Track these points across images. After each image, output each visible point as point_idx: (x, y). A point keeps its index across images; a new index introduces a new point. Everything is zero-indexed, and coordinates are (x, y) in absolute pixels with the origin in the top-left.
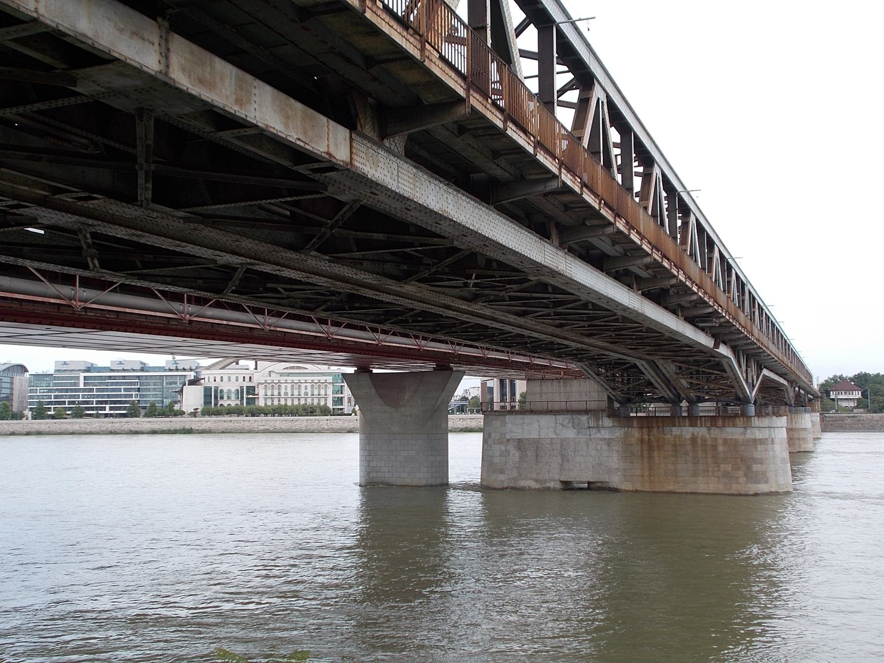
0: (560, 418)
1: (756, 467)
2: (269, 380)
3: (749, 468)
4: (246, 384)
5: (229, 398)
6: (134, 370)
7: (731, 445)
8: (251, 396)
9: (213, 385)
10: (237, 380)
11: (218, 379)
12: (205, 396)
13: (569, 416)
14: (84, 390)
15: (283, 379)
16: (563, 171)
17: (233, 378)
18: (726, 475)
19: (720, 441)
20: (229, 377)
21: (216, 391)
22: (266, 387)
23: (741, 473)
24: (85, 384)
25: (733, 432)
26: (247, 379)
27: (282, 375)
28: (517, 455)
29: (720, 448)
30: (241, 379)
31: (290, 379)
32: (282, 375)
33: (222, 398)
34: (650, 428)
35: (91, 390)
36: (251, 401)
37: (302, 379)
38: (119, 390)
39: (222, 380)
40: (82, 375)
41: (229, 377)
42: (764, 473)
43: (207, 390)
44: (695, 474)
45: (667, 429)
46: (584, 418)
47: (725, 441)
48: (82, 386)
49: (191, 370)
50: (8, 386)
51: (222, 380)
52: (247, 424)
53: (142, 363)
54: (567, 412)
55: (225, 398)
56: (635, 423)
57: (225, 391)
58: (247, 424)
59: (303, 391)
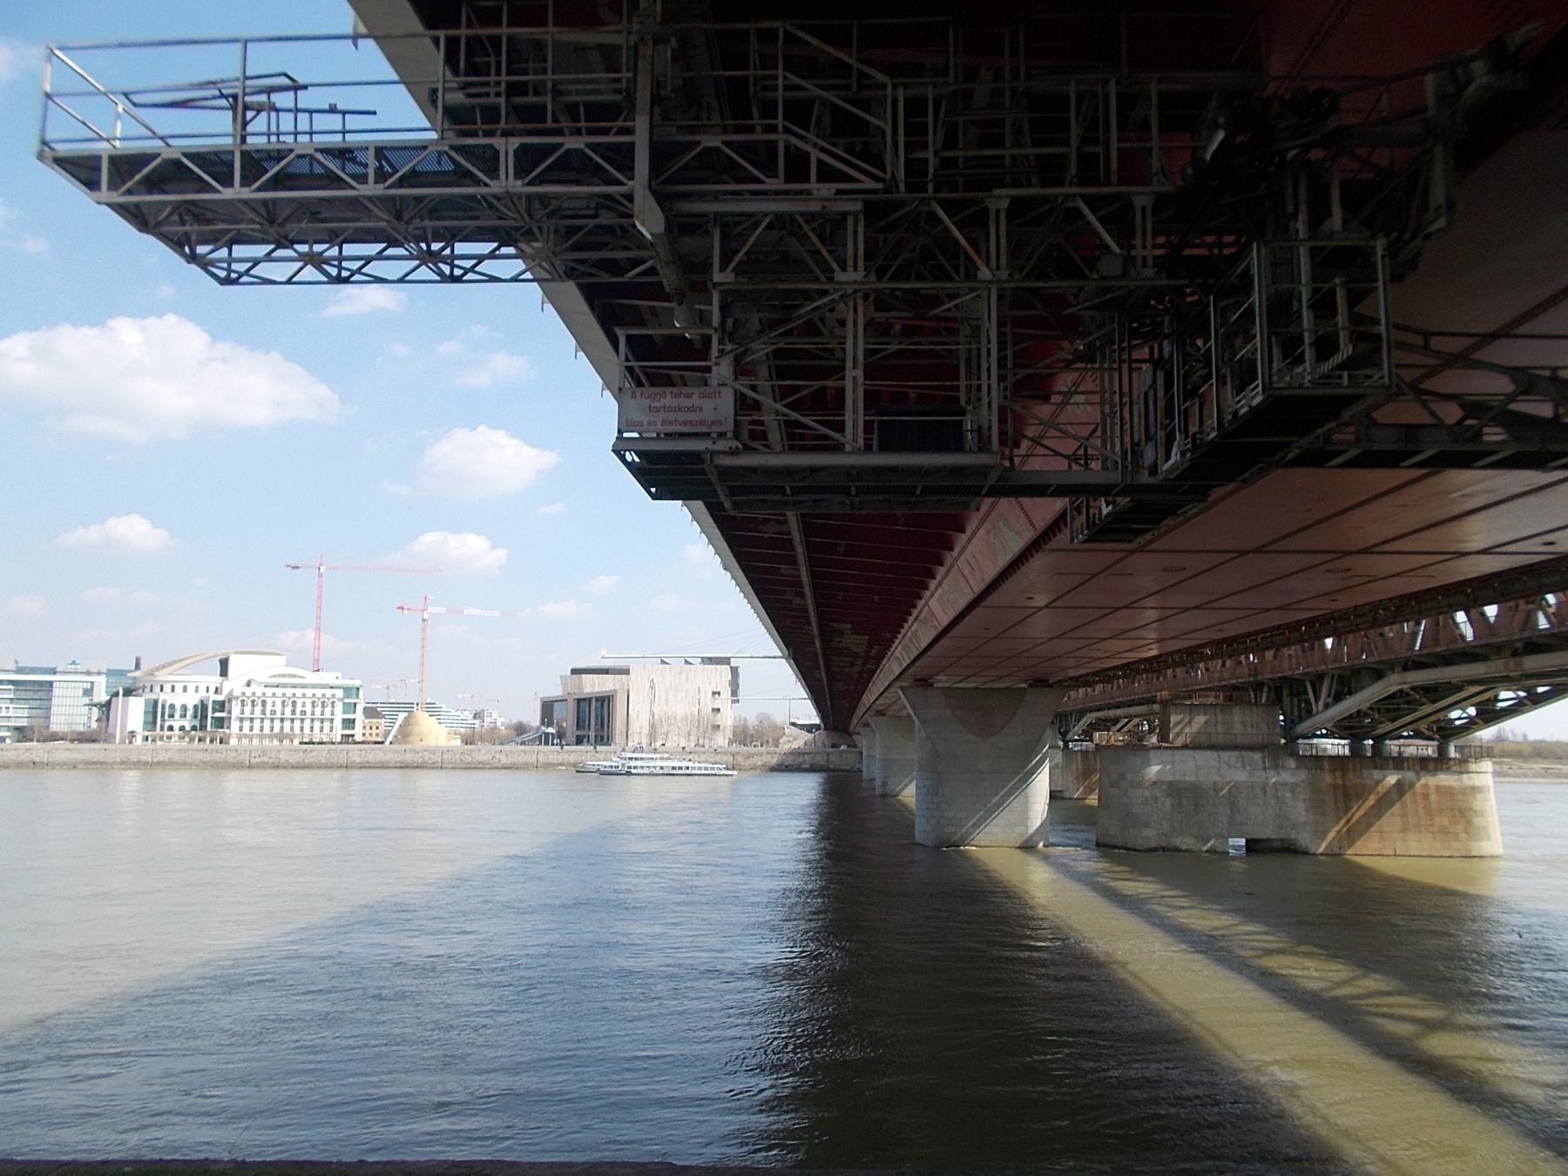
0: (1225, 755)
1: (1477, 821)
3: (1469, 822)
13: (1237, 753)
15: (269, 691)
16: (1434, 406)
17: (191, 688)
18: (1444, 831)
19: (1432, 791)
23: (1460, 828)
25: (1444, 779)
26: (212, 690)
28: (1168, 801)
29: (1433, 797)
31: (279, 691)
33: (171, 716)
34: (1344, 770)
37: (299, 692)
44: (1404, 830)
46: (1257, 756)
47: (1438, 788)
49: (99, 673)
54: (1236, 748)
55: (177, 716)
56: (1326, 766)
57: (178, 707)
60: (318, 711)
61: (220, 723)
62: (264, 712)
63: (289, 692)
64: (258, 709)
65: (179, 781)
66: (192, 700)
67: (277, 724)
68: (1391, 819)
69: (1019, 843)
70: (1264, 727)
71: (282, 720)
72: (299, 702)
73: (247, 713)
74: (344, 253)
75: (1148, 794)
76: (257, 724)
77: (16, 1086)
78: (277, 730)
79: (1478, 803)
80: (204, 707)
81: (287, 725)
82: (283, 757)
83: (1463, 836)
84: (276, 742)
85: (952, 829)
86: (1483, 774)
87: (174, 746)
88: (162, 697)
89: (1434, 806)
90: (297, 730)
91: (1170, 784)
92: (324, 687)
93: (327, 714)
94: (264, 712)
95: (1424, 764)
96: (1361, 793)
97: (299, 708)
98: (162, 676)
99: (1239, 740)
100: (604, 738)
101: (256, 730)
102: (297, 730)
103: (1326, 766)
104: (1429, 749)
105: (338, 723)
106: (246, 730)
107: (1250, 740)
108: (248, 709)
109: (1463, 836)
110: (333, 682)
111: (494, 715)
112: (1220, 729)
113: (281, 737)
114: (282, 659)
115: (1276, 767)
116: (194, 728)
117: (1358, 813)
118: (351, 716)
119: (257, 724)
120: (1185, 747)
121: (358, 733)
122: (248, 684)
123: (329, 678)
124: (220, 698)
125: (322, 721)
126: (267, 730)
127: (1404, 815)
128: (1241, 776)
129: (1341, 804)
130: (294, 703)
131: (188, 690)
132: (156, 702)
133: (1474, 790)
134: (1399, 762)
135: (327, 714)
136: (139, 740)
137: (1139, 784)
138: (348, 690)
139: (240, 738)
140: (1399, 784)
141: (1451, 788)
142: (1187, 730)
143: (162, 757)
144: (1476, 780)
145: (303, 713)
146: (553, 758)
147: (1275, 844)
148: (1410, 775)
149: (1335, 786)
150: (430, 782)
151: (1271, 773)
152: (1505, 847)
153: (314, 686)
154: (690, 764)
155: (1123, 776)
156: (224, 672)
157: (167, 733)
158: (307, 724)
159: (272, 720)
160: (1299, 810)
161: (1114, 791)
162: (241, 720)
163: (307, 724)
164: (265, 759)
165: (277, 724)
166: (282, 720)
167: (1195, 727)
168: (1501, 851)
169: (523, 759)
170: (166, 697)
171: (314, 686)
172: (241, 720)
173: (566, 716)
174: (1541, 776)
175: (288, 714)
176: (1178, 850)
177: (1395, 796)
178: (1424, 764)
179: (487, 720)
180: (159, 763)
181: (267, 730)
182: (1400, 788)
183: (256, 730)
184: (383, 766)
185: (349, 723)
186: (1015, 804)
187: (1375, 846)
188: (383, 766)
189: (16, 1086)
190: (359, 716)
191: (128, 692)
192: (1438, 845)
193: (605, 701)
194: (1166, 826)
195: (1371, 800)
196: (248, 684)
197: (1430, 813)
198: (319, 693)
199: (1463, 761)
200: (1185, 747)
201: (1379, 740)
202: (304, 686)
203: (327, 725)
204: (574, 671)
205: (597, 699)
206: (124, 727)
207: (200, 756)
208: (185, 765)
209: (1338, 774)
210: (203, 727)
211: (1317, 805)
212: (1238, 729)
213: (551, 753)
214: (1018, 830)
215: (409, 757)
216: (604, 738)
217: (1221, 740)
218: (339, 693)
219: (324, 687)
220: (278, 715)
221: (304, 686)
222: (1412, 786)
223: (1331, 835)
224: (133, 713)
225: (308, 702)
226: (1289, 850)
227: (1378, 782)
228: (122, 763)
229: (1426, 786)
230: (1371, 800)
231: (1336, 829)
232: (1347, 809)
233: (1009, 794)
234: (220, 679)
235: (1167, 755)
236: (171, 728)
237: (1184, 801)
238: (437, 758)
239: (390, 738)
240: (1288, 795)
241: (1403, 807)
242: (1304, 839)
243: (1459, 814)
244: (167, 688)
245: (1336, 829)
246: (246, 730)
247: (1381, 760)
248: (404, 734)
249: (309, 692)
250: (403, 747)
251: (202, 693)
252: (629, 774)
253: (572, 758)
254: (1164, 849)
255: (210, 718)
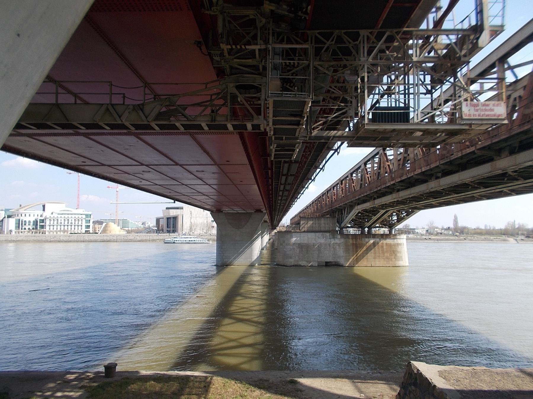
0: (317, 234)
1: (398, 255)
3: (396, 255)
4: (40, 218)
5: (29, 225)
7: (390, 246)
13: (321, 233)
15: (59, 216)
17: (32, 215)
18: (387, 258)
19: (385, 245)
21: (22, 221)
23: (393, 257)
25: (389, 241)
26: (39, 216)
28: (298, 250)
29: (385, 247)
31: (63, 216)
33: (25, 224)
34: (356, 239)
37: (70, 216)
42: (401, 257)
44: (375, 258)
45: (363, 239)
46: (328, 234)
47: (386, 244)
49: (2, 210)
50: (311, 207)
55: (27, 224)
56: (350, 237)
57: (27, 222)
60: (77, 222)
61: (42, 227)
62: (57, 223)
64: (55, 222)
65: (28, 248)
66: (32, 219)
67: (62, 227)
68: (371, 255)
69: (249, 264)
70: (331, 225)
71: (64, 226)
72: (59, 219)
73: (52, 223)
74: (426, 76)
75: (291, 247)
76: (55, 227)
78: (62, 229)
79: (399, 249)
80: (37, 221)
81: (66, 227)
82: (62, 238)
83: (394, 260)
84: (62, 233)
85: (227, 260)
86: (403, 239)
87: (25, 235)
88: (21, 218)
89: (385, 250)
90: (69, 229)
91: (299, 244)
92: (78, 214)
93: (80, 223)
94: (57, 223)
95: (383, 236)
96: (362, 246)
97: (70, 222)
98: (21, 211)
99: (323, 229)
101: (55, 229)
102: (69, 229)
103: (350, 237)
104: (385, 230)
105: (84, 227)
106: (52, 229)
107: (327, 229)
108: (52, 222)
109: (394, 260)
110: (82, 213)
111: (149, 223)
112: (317, 225)
113: (64, 231)
114: (64, 205)
115: (334, 238)
116: (33, 229)
117: (360, 253)
118: (88, 224)
119: (55, 227)
120: (304, 232)
121: (91, 230)
122: (52, 214)
123: (80, 211)
124: (42, 218)
125: (78, 226)
126: (59, 229)
127: (375, 253)
128: (322, 241)
129: (354, 250)
130: (68, 220)
131: (31, 216)
132: (19, 220)
133: (398, 244)
134: (375, 236)
135: (80, 223)
136: (13, 233)
137: (289, 244)
138: (87, 215)
139: (49, 232)
140: (374, 243)
141: (391, 244)
142: (306, 226)
143: (19, 239)
144: (399, 241)
145: (72, 223)
146: (155, 238)
147: (333, 263)
148: (378, 240)
149: (353, 244)
150: (114, 246)
151: (332, 240)
152: (409, 263)
153: (75, 214)
154: (195, 239)
155: (284, 242)
156: (44, 210)
157: (23, 230)
158: (73, 227)
159: (61, 226)
160: (341, 252)
161: (281, 247)
162: (50, 226)
163: (73, 227)
164: (55, 239)
165: (62, 227)
166: (64, 226)
167: (309, 225)
168: (407, 264)
169: (145, 238)
170: (23, 218)
171: (75, 214)
172: (50, 226)
173: (163, 223)
174: (484, 240)
175: (66, 224)
176: (300, 266)
177: (372, 247)
178: (383, 236)
179: (147, 225)
180: (18, 241)
181: (59, 229)
182: (374, 244)
183: (55, 229)
184: (96, 241)
185: (88, 227)
186: (248, 251)
187: (365, 263)
188: (96, 241)
190: (91, 224)
191: (9, 217)
192: (385, 262)
193: (175, 218)
194: (297, 258)
195: (365, 248)
196: (52, 214)
197: (383, 253)
198: (77, 216)
199: (395, 235)
200: (304, 232)
201: (370, 228)
202: (72, 214)
203: (80, 227)
204: (167, 208)
205: (173, 218)
206: (8, 228)
207: (33, 238)
208: (28, 241)
209: (354, 240)
210: (36, 228)
211: (347, 250)
212: (323, 225)
213: (154, 236)
214: (249, 260)
215: (105, 238)
217: (317, 229)
218: (84, 216)
219: (78, 214)
220: (63, 224)
221: (72, 214)
222: (378, 243)
223: (351, 260)
224: (11, 224)
225: (63, 220)
226: (337, 265)
227: (367, 242)
228: (5, 241)
229: (383, 243)
230: (365, 248)
231: (353, 258)
232: (357, 251)
233: (246, 248)
234: (42, 212)
235: (298, 234)
236: (25, 229)
237: (303, 250)
238: (115, 238)
239: (100, 232)
240: (337, 247)
241: (375, 251)
242: (342, 261)
243: (393, 252)
244: (23, 215)
245: (353, 258)
246: (52, 229)
247: (370, 235)
248: (105, 231)
249: (73, 216)
250: (104, 234)
251: (36, 217)
252: (174, 243)
253: (162, 238)
254: (296, 266)
255: (39, 225)
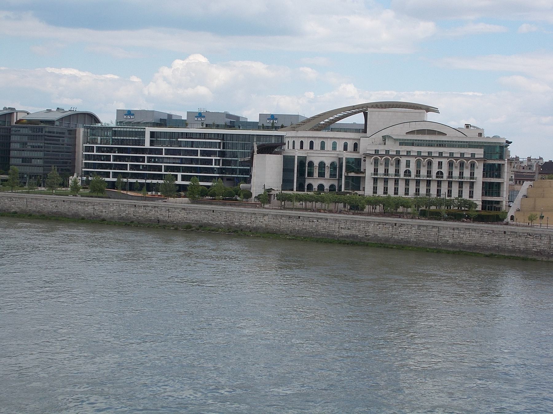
2: (382, 149)
4: (346, 155)
5: (321, 175)
6: (218, 127)
8: (353, 174)
9: (298, 153)
10: (334, 148)
11: (306, 145)
12: (284, 170)
14: (150, 151)
15: (403, 149)
17: (329, 145)
20: (302, 143)
22: (376, 162)
24: (152, 143)
26: (350, 147)
27: (403, 143)
30: (340, 147)
31: (414, 150)
32: (403, 143)
33: (311, 174)
35: (160, 152)
36: (356, 183)
37: (435, 150)
38: (108, 158)
39: (311, 147)
40: (148, 130)
41: (302, 143)
43: (288, 161)
48: (147, 145)
51: (311, 147)
52: (323, 224)
53: (228, 116)
55: (316, 174)
57: (316, 164)
58: (323, 224)
59: (435, 169)
63: (425, 150)
77: (411, 229)
100: (439, 162)
189: (411, 229)
198: (457, 152)
202: (441, 144)
216: (439, 162)
221: (441, 144)
249: (446, 151)
